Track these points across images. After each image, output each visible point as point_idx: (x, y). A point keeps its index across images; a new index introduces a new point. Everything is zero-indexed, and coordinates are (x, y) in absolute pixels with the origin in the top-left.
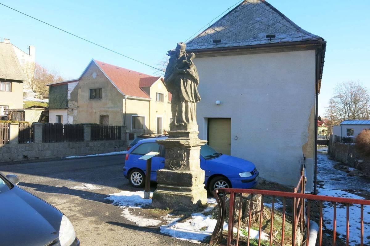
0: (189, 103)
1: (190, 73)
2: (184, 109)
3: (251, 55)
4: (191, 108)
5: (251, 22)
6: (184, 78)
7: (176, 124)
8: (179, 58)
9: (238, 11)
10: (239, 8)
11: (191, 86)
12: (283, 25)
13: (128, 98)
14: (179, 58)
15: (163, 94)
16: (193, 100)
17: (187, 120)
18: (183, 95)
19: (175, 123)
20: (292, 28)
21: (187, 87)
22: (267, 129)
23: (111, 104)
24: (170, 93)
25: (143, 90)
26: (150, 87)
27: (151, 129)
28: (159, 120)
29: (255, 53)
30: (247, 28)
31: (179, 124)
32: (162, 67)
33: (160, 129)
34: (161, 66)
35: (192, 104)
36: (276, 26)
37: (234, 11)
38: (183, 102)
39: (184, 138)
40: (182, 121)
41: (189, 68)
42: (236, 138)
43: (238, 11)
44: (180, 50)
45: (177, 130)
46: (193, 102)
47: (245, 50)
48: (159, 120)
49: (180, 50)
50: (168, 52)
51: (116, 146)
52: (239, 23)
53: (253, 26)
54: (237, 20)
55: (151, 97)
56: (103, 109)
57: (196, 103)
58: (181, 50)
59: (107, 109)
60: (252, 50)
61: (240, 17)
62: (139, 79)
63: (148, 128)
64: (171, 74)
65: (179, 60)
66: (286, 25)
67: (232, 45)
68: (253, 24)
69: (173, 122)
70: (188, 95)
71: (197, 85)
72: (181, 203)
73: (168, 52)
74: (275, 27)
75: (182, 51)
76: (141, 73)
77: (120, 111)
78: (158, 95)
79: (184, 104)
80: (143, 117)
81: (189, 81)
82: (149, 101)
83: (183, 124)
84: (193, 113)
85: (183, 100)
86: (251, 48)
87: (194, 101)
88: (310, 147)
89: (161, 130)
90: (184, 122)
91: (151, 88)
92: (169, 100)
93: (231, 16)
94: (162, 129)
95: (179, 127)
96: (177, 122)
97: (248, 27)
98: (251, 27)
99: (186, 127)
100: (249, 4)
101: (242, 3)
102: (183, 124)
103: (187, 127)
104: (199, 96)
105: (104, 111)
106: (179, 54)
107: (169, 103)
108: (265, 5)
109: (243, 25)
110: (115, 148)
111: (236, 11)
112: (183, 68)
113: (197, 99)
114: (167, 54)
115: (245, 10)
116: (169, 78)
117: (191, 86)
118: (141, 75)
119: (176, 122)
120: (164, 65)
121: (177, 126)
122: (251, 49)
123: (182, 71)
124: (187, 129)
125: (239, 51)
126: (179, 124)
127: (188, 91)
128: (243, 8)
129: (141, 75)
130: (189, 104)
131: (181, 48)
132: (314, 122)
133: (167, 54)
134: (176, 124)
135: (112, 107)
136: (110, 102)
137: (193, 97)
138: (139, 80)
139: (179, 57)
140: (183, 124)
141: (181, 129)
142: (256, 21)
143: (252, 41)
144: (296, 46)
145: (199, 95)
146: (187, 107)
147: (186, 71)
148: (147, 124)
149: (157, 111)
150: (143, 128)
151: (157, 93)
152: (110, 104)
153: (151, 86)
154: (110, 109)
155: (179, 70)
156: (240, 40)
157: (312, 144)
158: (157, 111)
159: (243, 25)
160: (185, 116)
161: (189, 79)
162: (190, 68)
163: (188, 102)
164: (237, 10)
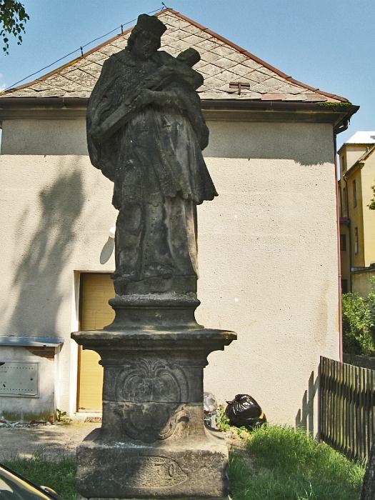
22: (236, 300)
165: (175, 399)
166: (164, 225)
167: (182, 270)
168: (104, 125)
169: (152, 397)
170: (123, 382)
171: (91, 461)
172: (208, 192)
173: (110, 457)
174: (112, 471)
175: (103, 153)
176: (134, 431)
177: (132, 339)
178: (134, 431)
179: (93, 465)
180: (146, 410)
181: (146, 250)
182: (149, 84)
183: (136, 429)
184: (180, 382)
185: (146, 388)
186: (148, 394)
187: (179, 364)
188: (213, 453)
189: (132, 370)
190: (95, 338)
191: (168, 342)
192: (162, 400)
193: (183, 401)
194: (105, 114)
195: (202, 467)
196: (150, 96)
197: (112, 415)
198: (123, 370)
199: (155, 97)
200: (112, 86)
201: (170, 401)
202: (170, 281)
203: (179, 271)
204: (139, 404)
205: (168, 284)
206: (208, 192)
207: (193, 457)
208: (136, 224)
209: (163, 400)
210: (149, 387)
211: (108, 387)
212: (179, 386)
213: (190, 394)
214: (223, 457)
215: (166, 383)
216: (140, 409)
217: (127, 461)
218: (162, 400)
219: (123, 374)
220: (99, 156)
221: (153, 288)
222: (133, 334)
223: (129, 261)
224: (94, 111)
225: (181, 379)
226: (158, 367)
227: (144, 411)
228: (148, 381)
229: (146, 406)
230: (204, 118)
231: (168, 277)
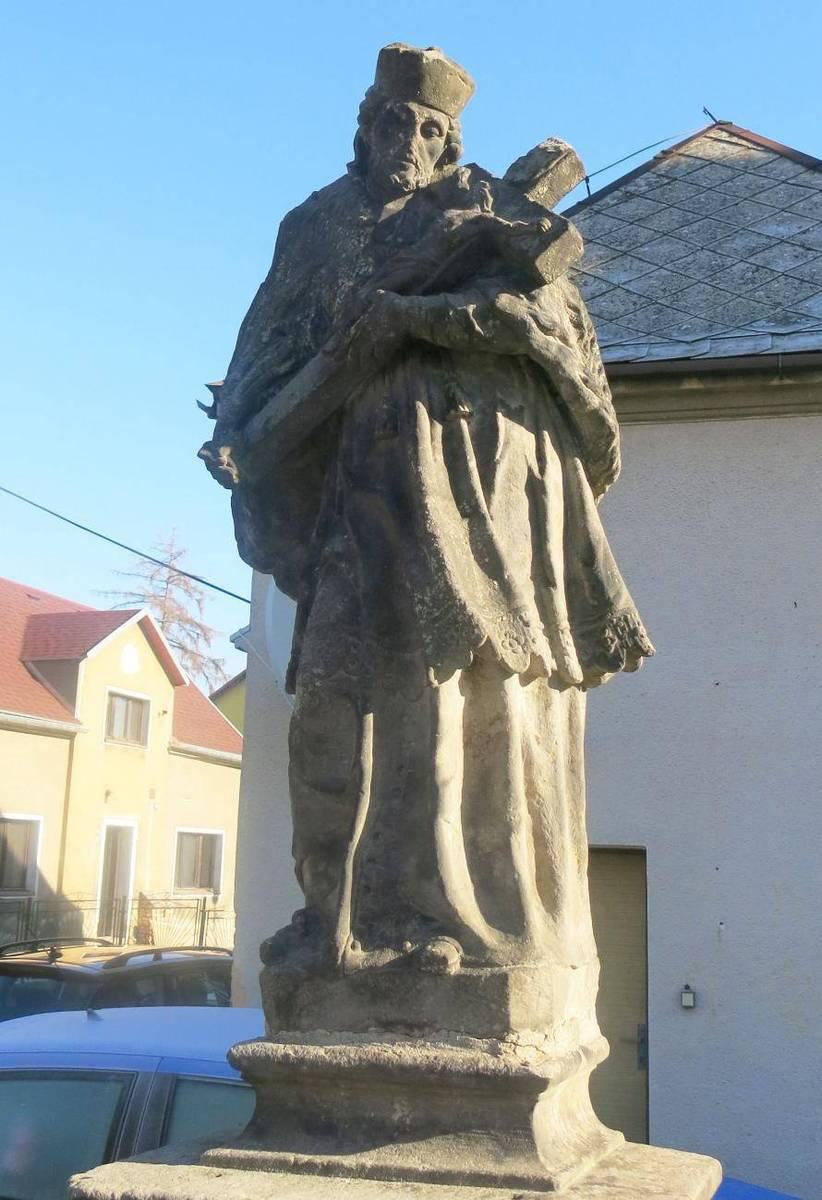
0: (513, 684)
1: (538, 337)
2: (451, 760)
3: (774, 423)
4: (537, 751)
5: (739, 243)
6: (452, 403)
7: (352, 951)
8: (394, 206)
9: (642, 195)
11: (535, 490)
14: (394, 206)
15: (148, 702)
16: (558, 651)
17: (504, 904)
18: (449, 592)
19: (345, 935)
21: (497, 497)
24: (270, 581)
25: (39, 675)
26: (79, 661)
27: (70, 891)
28: (116, 845)
29: (775, 412)
30: (714, 271)
31: (389, 956)
32: (147, 587)
33: (118, 894)
34: (141, 579)
35: (547, 706)
37: (617, 193)
38: (443, 676)
39: (468, 1164)
40: (426, 919)
41: (529, 282)
42: (688, 1000)
43: (642, 195)
44: (414, 106)
45: (357, 1030)
46: (560, 680)
47: (740, 383)
48: (116, 845)
49: (414, 106)
50: (211, 387)
52: (665, 248)
53: (758, 260)
54: (644, 234)
55: (78, 714)
57: (582, 697)
58: (421, 114)
60: (790, 388)
61: (663, 221)
62: (25, 621)
63: (53, 884)
64: (292, 372)
65: (393, 218)
67: (649, 354)
68: (752, 252)
69: (314, 925)
70: (506, 591)
71: (596, 496)
73: (211, 387)
75: (430, 127)
76: (38, 592)
78: (120, 704)
79: (452, 699)
80: (29, 827)
81: (516, 442)
82: (70, 736)
83: (444, 960)
84: (558, 811)
85: (457, 641)
87: (577, 671)
89: (125, 898)
90: (455, 928)
91: (82, 665)
92: (174, 735)
93: (601, 218)
94: (132, 894)
95: (403, 994)
96: (365, 933)
97: (723, 268)
98: (742, 266)
99: (484, 1004)
100: (698, 162)
101: (657, 160)
102: (452, 953)
103: (502, 998)
104: (636, 617)
106: (402, 159)
107: (174, 749)
108: (800, 168)
109: (689, 259)
111: (629, 196)
112: (451, 288)
113: (603, 643)
114: (201, 405)
115: (680, 191)
116: (282, 404)
117: (535, 490)
118: (37, 599)
119: (357, 932)
120: (158, 577)
121: (368, 984)
122: (775, 382)
123: (440, 314)
124: (497, 1028)
125: (692, 393)
126: (389, 956)
127: (502, 543)
129: (37, 599)
130: (520, 699)
131: (428, 83)
132: (627, 844)
133: (201, 405)
134: (352, 951)
137: (565, 623)
138: (20, 624)
139: (397, 192)
140: (455, 967)
141: (412, 1029)
142: (765, 241)
143: (773, 334)
145: (625, 601)
146: (489, 740)
147: (489, 312)
148: (45, 864)
149: (108, 794)
150: (22, 886)
151: (112, 695)
153: (84, 655)
155: (402, 302)
156: (687, 332)
158: (108, 794)
159: (689, 259)
160: (473, 847)
161: (515, 416)
162: (540, 282)
163: (507, 672)
164: (631, 188)
196: (395, 314)
221: (390, 1012)
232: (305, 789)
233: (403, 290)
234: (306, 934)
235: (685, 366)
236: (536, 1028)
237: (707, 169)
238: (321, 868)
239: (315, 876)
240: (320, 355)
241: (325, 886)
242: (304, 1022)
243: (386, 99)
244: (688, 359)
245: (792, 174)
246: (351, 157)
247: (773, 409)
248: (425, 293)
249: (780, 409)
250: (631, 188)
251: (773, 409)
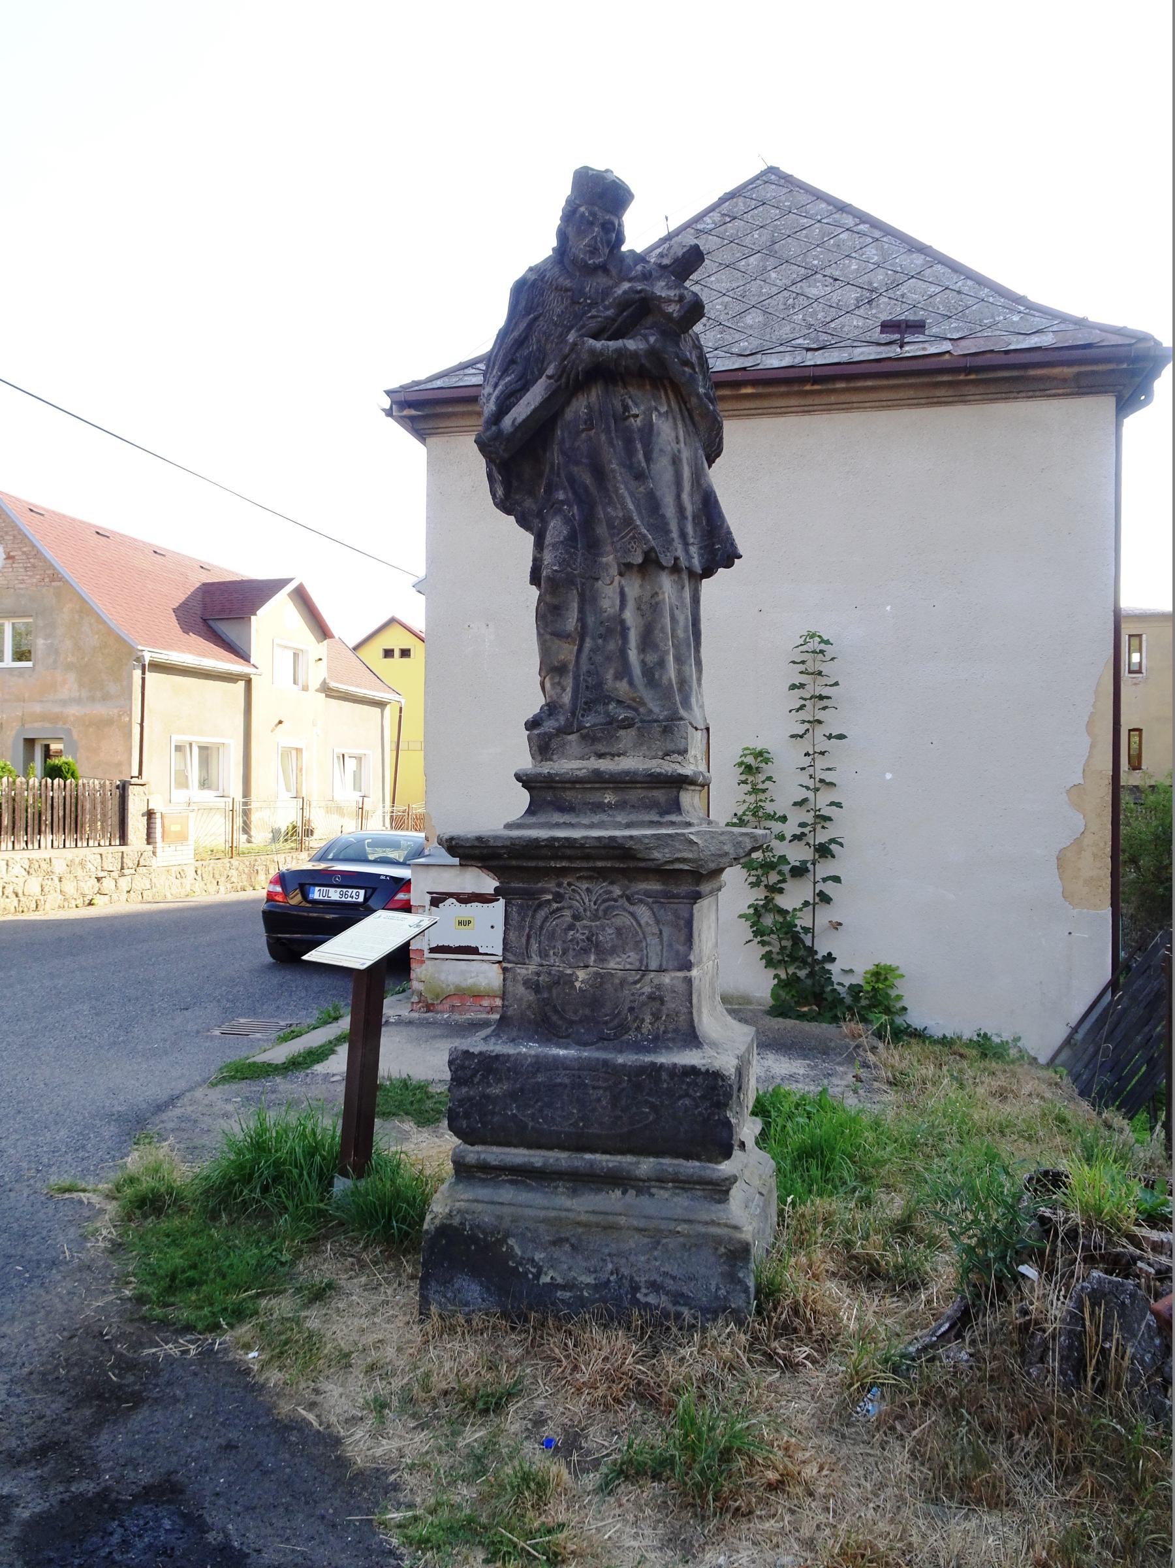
3: (806, 418)
10: (707, 219)
11: (676, 461)
12: (941, 289)
13: (157, 667)
20: (991, 300)
22: (889, 776)
23: (76, 686)
29: (829, 408)
36: (903, 289)
51: (101, 874)
56: (38, 708)
59: (57, 709)
66: (956, 287)
72: (654, 1287)
74: (903, 296)
77: (120, 716)
86: (815, 380)
88: (1095, 856)
105: (44, 718)
110: (99, 879)
122: (808, 387)
128: (728, 219)
135: (78, 701)
136: (72, 677)
144: (1032, 372)
149: (280, 722)
152: (69, 686)
154: (73, 711)
155: (598, 345)
157: (1102, 845)
158: (280, 722)
165: (637, 964)
166: (622, 622)
167: (656, 710)
168: (507, 422)
169: (593, 958)
170: (541, 928)
171: (474, 1075)
172: (720, 552)
173: (509, 1070)
174: (513, 1095)
175: (515, 484)
176: (560, 1022)
177: (546, 846)
178: (560, 1022)
179: (478, 1083)
180: (582, 982)
181: (588, 672)
182: (592, 325)
183: (562, 1018)
184: (648, 930)
185: (583, 940)
186: (586, 951)
187: (645, 895)
188: (703, 1069)
189: (555, 905)
190: (476, 844)
191: (618, 852)
192: (612, 965)
193: (654, 965)
194: (505, 405)
195: (680, 1097)
196: (592, 351)
197: (521, 990)
198: (540, 906)
199: (601, 354)
200: (526, 338)
201: (628, 967)
202: (632, 732)
203: (651, 711)
204: (569, 971)
205: (627, 737)
206: (720, 552)
207: (664, 1076)
208: (571, 622)
209: (613, 964)
210: (588, 938)
211: (512, 936)
212: (645, 938)
213: (665, 954)
214: (723, 1080)
215: (619, 931)
216: (569, 981)
217: (540, 1078)
218: (612, 965)
219: (542, 914)
220: (507, 494)
221: (602, 749)
222: (546, 836)
223: (560, 696)
224: (490, 394)
225: (647, 923)
226: (604, 901)
227: (578, 984)
228: (585, 927)
229: (581, 974)
230: (705, 402)
231: (627, 724)
232: (548, 637)
233: (596, 336)
234: (550, 715)
235: (740, 376)
236: (679, 753)
237: (761, 209)
238: (557, 680)
239: (553, 685)
240: (544, 377)
241: (559, 690)
242: (555, 757)
243: (580, 206)
244: (744, 369)
245: (826, 214)
246: (554, 243)
247: (806, 408)
248: (609, 339)
249: (811, 408)
250: (700, 226)
251: (806, 408)
